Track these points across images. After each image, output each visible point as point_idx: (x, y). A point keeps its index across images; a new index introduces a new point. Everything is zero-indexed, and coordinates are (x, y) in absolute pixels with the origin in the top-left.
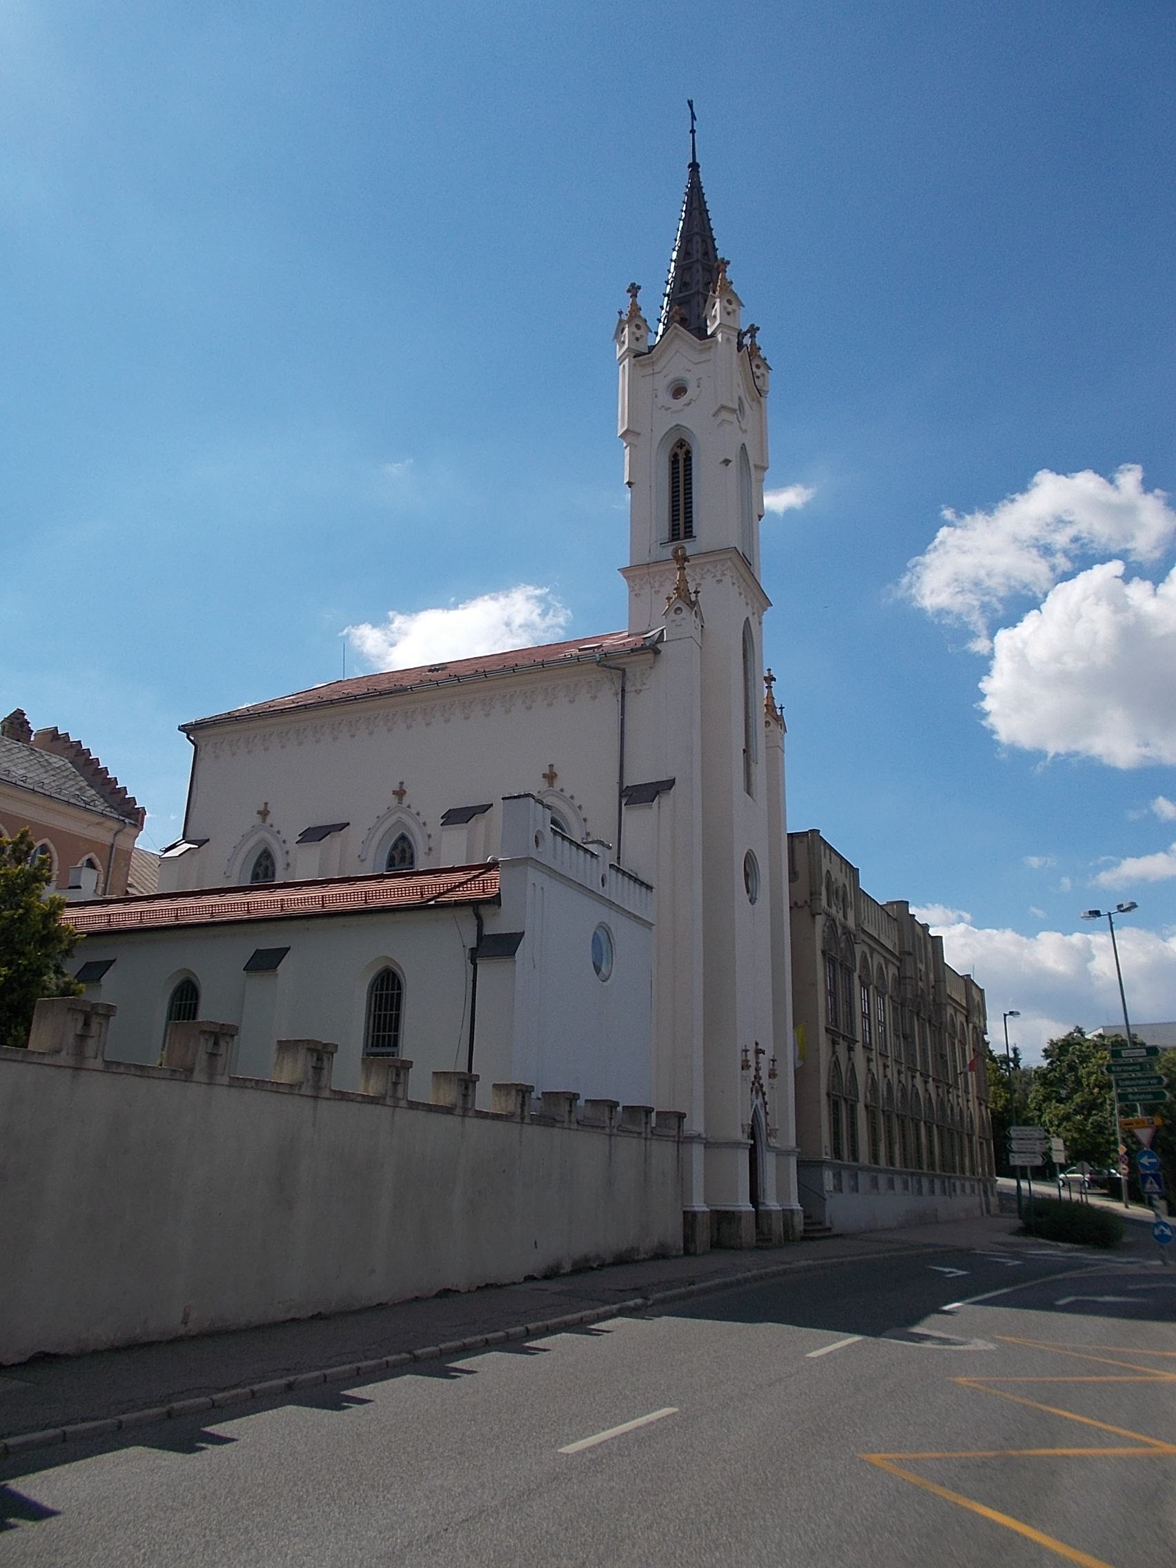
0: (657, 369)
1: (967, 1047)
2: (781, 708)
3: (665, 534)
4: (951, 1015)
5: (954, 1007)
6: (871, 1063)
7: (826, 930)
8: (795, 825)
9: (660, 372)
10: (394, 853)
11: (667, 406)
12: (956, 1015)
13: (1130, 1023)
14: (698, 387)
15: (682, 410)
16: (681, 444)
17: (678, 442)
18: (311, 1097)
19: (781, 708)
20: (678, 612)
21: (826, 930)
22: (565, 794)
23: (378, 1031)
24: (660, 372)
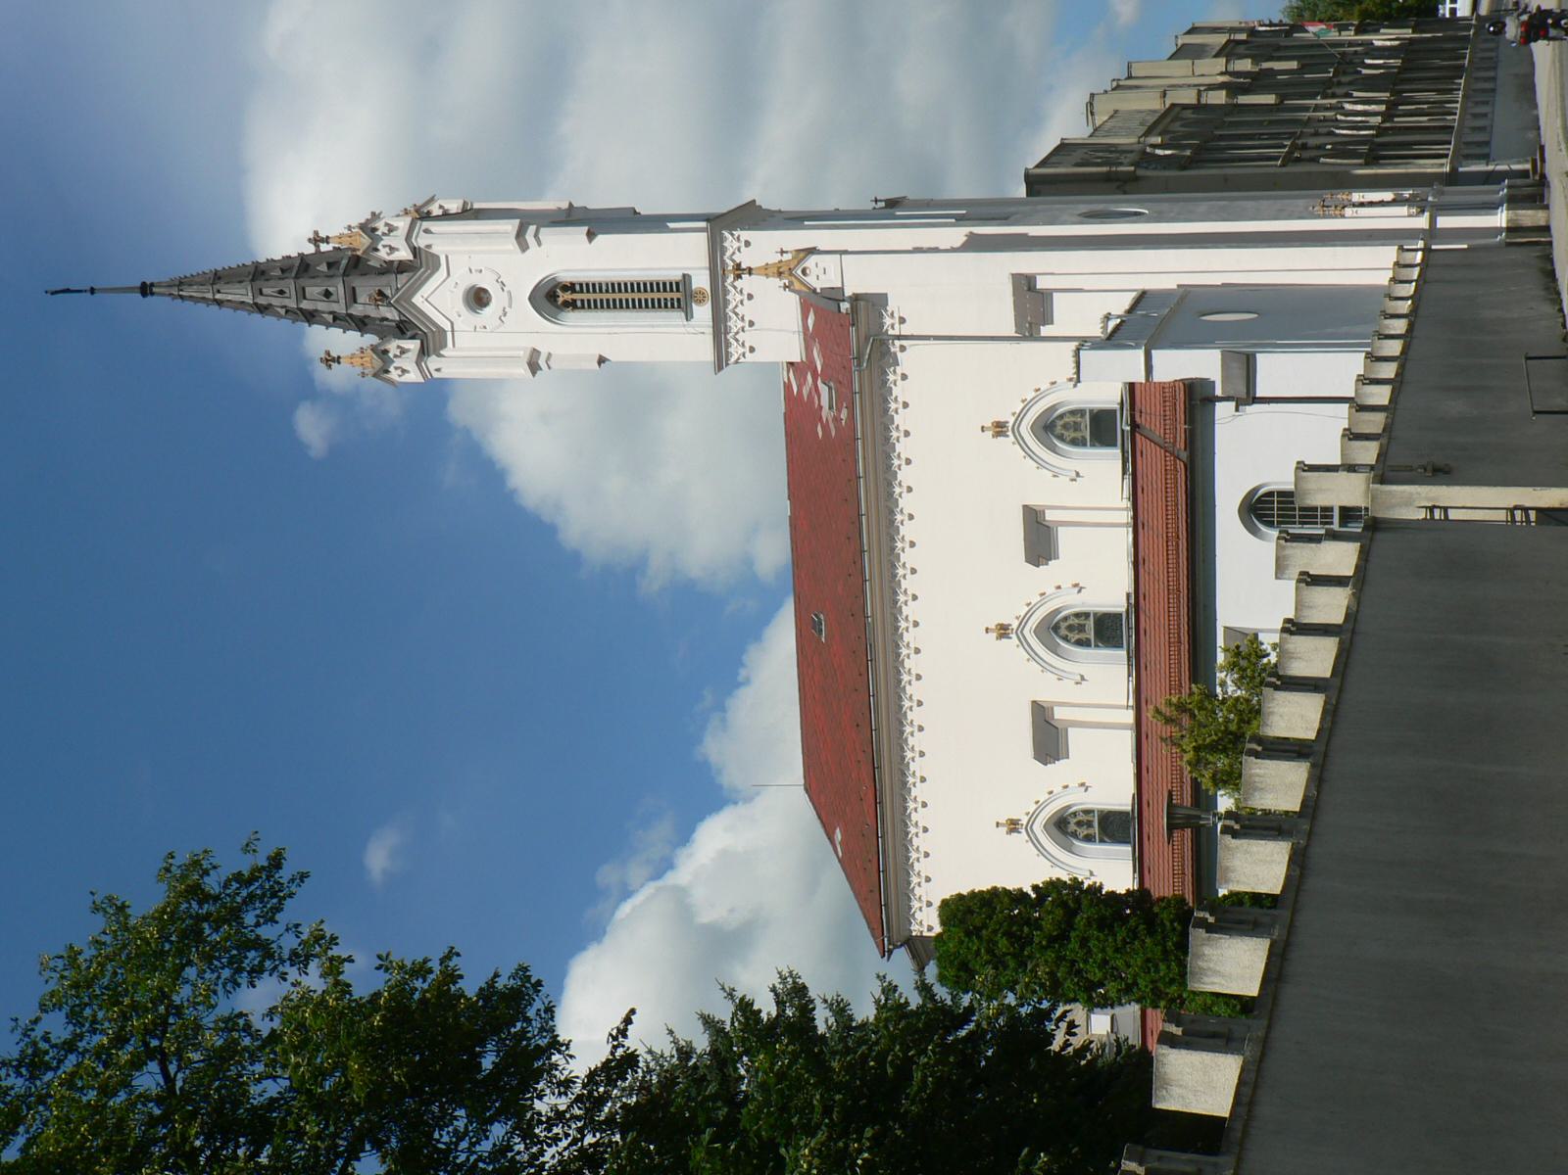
0: (447, 326)
1: (1282, 44)
2: (876, 201)
3: (677, 316)
4: (1182, 126)
5: (1172, 121)
6: (1309, 145)
7: (1154, 166)
8: (1021, 191)
9: (452, 324)
10: (1073, 640)
11: (501, 313)
12: (1174, 132)
13: (455, 329)
14: (481, 271)
15: (509, 293)
16: (552, 296)
17: (549, 301)
18: (1271, 1019)
19: (876, 201)
20: (808, 271)
21: (1154, 166)
22: (1042, 389)
23: (1316, 517)
24: (452, 324)
